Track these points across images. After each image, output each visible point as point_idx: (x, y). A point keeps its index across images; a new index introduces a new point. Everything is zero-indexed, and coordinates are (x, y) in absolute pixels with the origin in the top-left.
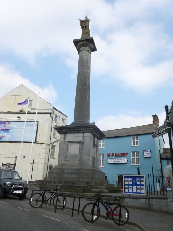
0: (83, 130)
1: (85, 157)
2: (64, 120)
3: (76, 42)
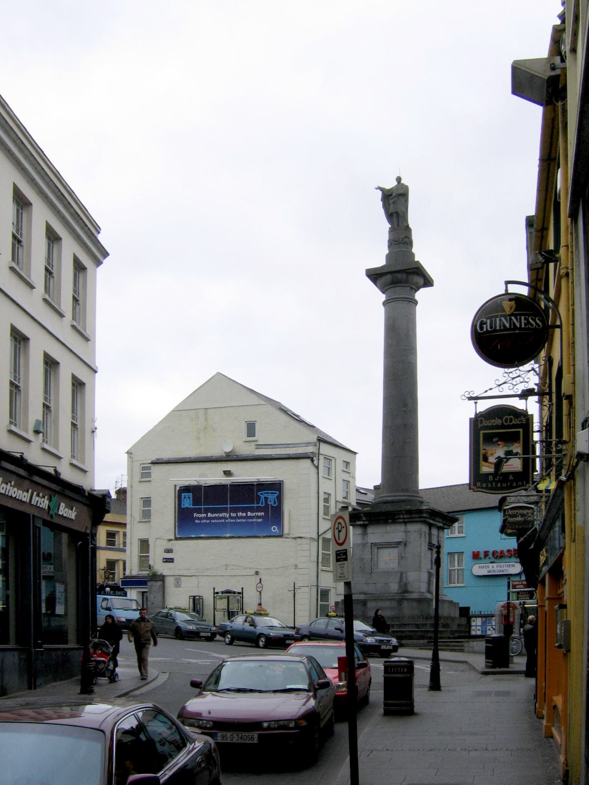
0: (404, 518)
1: (412, 576)
2: (349, 463)
3: (374, 275)
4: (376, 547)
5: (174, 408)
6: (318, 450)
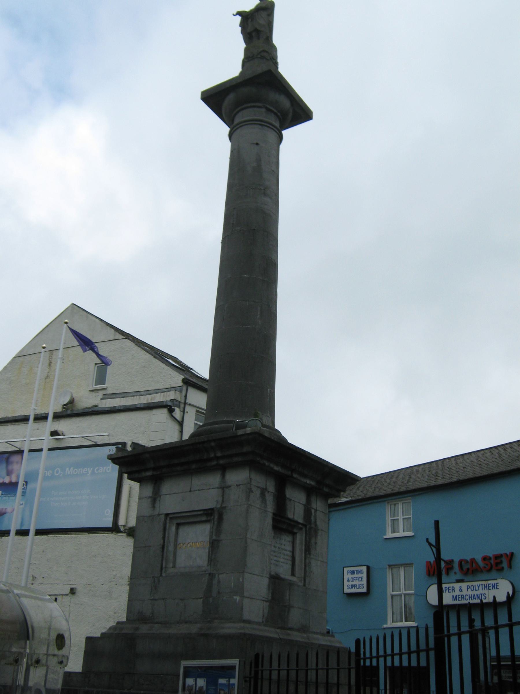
0: (218, 458)
4: (175, 522)
5: (16, 354)
6: (183, 398)
